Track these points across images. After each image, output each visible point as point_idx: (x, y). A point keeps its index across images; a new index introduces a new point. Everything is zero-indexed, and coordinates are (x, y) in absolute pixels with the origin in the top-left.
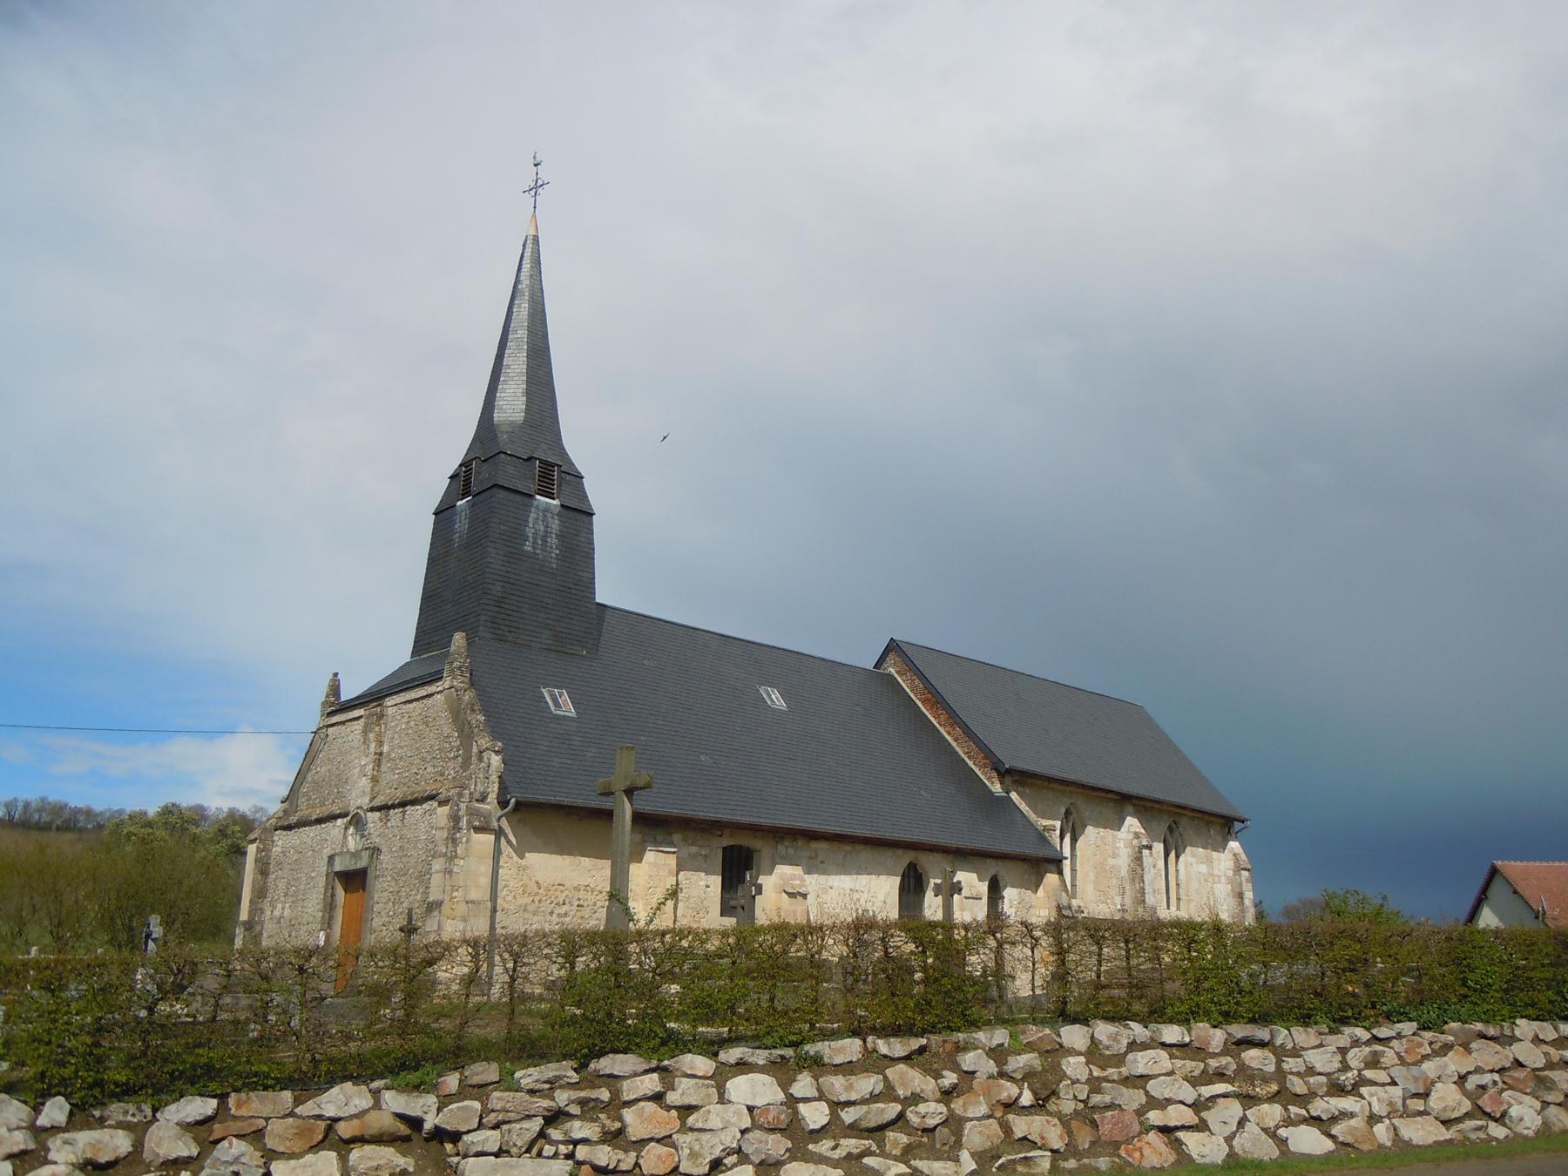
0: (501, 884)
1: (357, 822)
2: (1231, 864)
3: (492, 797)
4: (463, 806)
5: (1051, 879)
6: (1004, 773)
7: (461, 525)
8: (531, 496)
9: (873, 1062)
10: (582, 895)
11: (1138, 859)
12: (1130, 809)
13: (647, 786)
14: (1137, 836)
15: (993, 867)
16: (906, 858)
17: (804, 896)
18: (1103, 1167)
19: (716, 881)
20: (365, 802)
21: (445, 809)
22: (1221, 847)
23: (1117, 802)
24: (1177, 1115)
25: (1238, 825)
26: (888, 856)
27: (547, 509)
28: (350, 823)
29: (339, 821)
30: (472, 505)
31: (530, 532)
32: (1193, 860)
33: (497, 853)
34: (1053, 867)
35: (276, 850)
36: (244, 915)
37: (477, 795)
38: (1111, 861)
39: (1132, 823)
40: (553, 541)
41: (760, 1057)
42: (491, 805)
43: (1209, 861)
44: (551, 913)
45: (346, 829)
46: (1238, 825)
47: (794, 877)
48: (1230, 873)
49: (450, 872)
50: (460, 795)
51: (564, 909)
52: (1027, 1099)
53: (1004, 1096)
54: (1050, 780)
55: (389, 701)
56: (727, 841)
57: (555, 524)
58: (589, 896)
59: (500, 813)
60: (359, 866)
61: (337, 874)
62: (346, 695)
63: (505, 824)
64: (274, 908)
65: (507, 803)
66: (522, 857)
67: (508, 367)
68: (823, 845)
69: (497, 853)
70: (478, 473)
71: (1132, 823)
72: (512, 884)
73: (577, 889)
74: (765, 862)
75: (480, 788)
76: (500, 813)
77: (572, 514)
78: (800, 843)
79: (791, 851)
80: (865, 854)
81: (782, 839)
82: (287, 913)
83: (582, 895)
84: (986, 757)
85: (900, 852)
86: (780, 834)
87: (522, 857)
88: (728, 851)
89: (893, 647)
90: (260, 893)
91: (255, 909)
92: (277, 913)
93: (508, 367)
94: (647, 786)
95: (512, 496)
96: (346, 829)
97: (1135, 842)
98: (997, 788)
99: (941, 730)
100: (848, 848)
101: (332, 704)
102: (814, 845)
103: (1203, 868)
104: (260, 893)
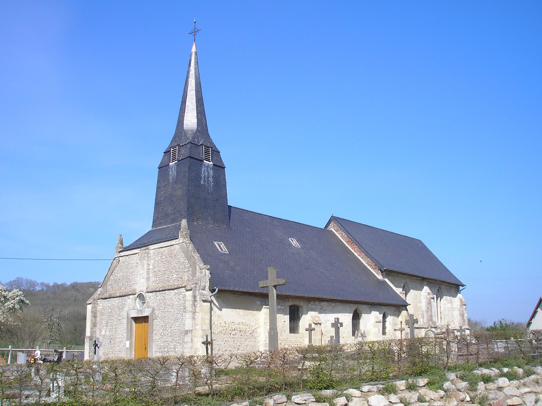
0: (213, 323)
1: (141, 297)
2: (459, 303)
3: (207, 287)
4: (197, 292)
5: (404, 313)
6: (387, 273)
7: (172, 173)
8: (202, 161)
9: (411, 388)
10: (241, 326)
11: (429, 303)
12: (425, 283)
14: (429, 294)
15: (385, 309)
16: (354, 307)
17: (320, 324)
19: (287, 317)
20: (144, 289)
21: (190, 293)
22: (455, 296)
23: (421, 281)
25: (461, 288)
26: (348, 306)
27: (208, 166)
29: (131, 296)
30: (177, 165)
31: (203, 176)
32: (446, 302)
33: (211, 309)
34: (404, 308)
35: (99, 308)
36: (88, 333)
38: (419, 305)
39: (426, 289)
40: (211, 179)
41: (375, 389)
42: (207, 292)
43: (451, 302)
45: (135, 300)
46: (461, 288)
47: (316, 317)
48: (459, 307)
49: (194, 318)
50: (196, 287)
52: (468, 399)
53: (461, 397)
54: (398, 273)
55: (152, 247)
56: (291, 303)
57: (211, 173)
58: (243, 327)
59: (211, 294)
61: (133, 318)
62: (126, 244)
63: (213, 298)
65: (214, 290)
67: (189, 106)
68: (325, 303)
69: (211, 309)
70: (179, 151)
71: (426, 289)
72: (216, 323)
74: (305, 311)
75: (203, 284)
77: (217, 168)
78: (317, 303)
79: (314, 306)
80: (340, 306)
81: (310, 301)
82: (108, 333)
83: (241, 326)
84: (376, 265)
85: (352, 305)
86: (309, 300)
88: (291, 307)
89: (333, 219)
91: (93, 332)
92: (103, 333)
93: (189, 106)
95: (195, 161)
96: (135, 300)
97: (428, 296)
98: (380, 277)
99: (356, 254)
100: (334, 304)
101: (120, 248)
102: (322, 303)
103: (449, 305)
104: (94, 325)
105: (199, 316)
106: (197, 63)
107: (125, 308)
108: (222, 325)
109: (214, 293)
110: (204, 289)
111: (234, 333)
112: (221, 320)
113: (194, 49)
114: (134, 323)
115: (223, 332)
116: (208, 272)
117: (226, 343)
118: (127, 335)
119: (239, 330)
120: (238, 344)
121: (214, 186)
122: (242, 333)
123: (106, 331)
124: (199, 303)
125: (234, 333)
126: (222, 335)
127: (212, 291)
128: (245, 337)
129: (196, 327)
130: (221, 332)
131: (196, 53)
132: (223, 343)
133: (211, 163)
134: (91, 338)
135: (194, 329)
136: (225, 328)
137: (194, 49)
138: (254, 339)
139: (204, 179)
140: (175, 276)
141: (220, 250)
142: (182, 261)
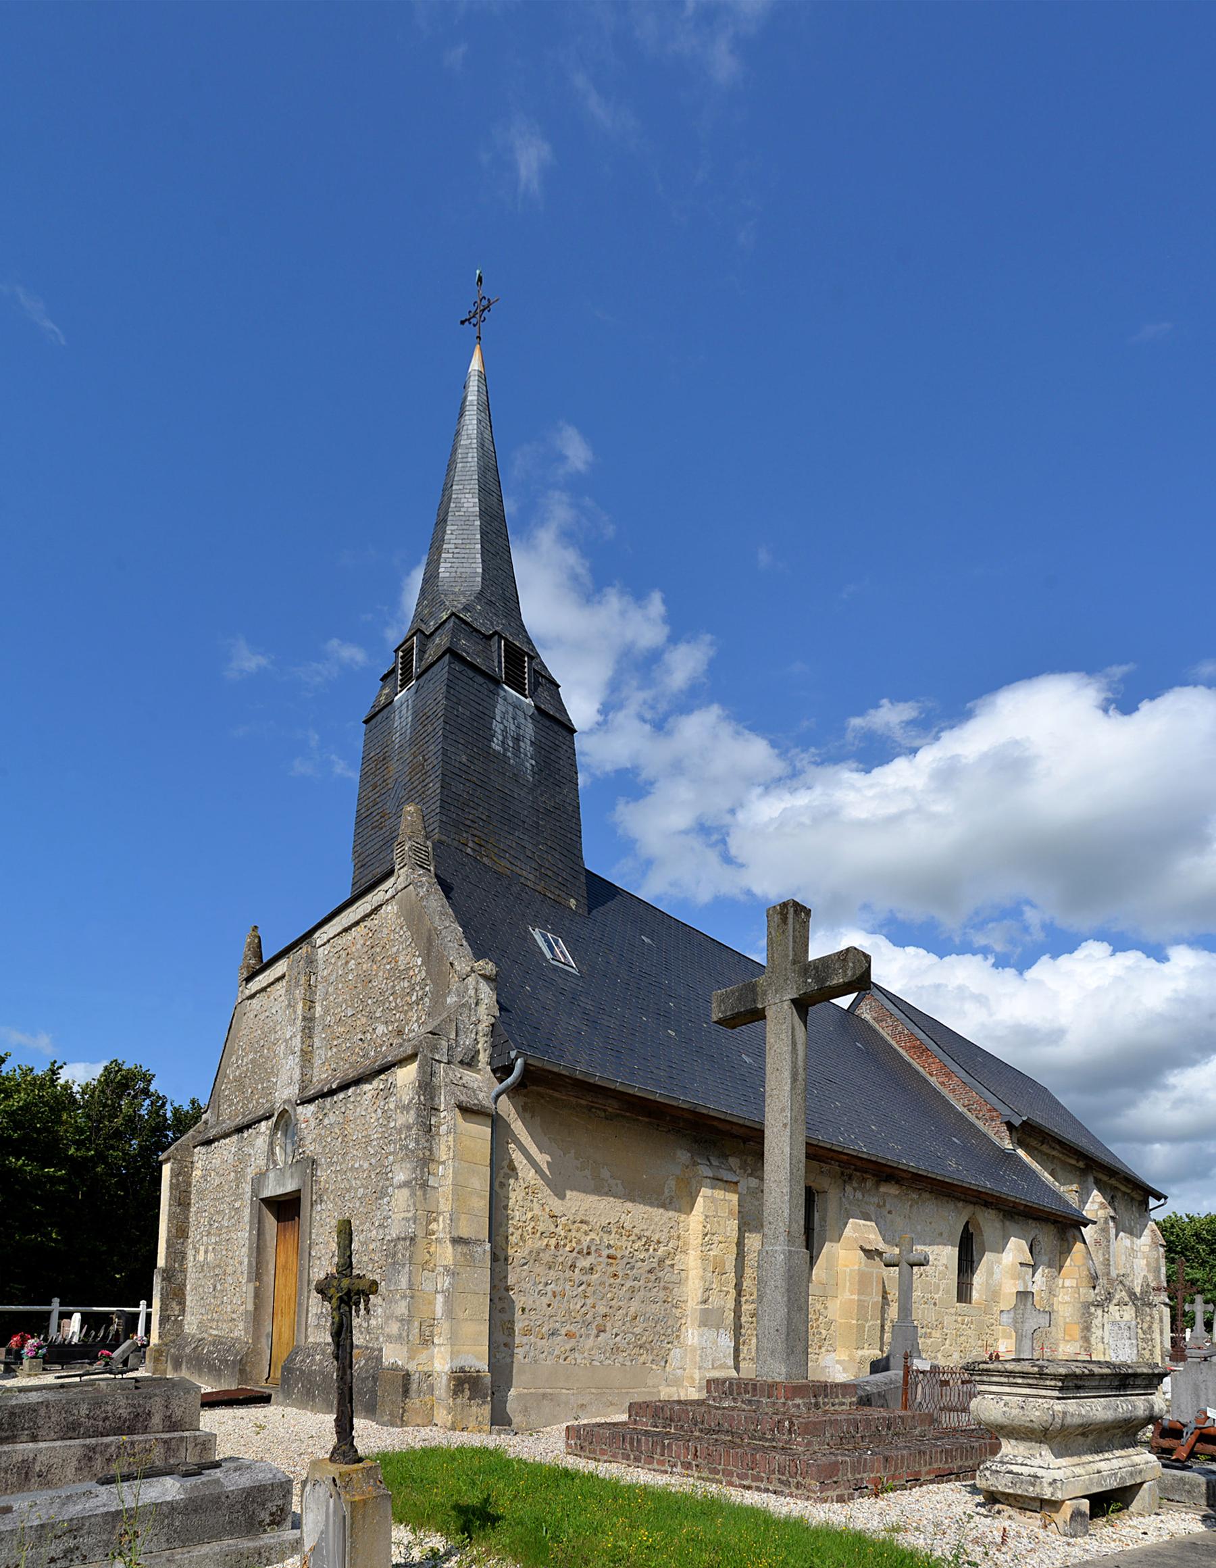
1: (284, 1122)
3: (483, 1057)
10: (612, 1239)
13: (964, 1293)
18: (400, 1533)
24: (402, 1549)
27: (517, 706)
28: (276, 1126)
31: (497, 727)
36: (161, 1262)
37: (459, 1053)
40: (527, 747)
42: (481, 1083)
44: (573, 1267)
51: (590, 1260)
58: (623, 1242)
60: (1204, 1487)
63: (506, 1107)
64: (197, 1251)
66: (562, 1197)
73: (606, 1229)
76: (499, 1087)
79: (859, 1195)
82: (211, 1256)
83: (612, 1239)
87: (562, 1197)
90: (180, 1232)
92: (201, 1257)
94: (964, 1293)
105: (444, 1175)
106: (486, 407)
107: (249, 1170)
108: (541, 1229)
109: (510, 1080)
110: (470, 1062)
111: (585, 1263)
112: (537, 1211)
113: (476, 365)
114: (271, 1221)
115: (546, 1257)
116: (487, 994)
117: (555, 1304)
118: (249, 1261)
119: (605, 1253)
120: (602, 1310)
121: (538, 771)
122: (619, 1268)
123: (206, 1252)
124: (447, 1118)
125: (585, 1263)
126: (539, 1269)
127: (501, 1071)
128: (629, 1284)
129: (433, 1226)
130: (536, 1256)
131: (483, 377)
132: (545, 1300)
133: (528, 701)
134: (168, 1275)
135: (421, 1234)
136: (553, 1242)
137: (476, 365)
138: (662, 1294)
139: (505, 738)
140: (381, 1029)
141: (549, 955)
142: (403, 960)
